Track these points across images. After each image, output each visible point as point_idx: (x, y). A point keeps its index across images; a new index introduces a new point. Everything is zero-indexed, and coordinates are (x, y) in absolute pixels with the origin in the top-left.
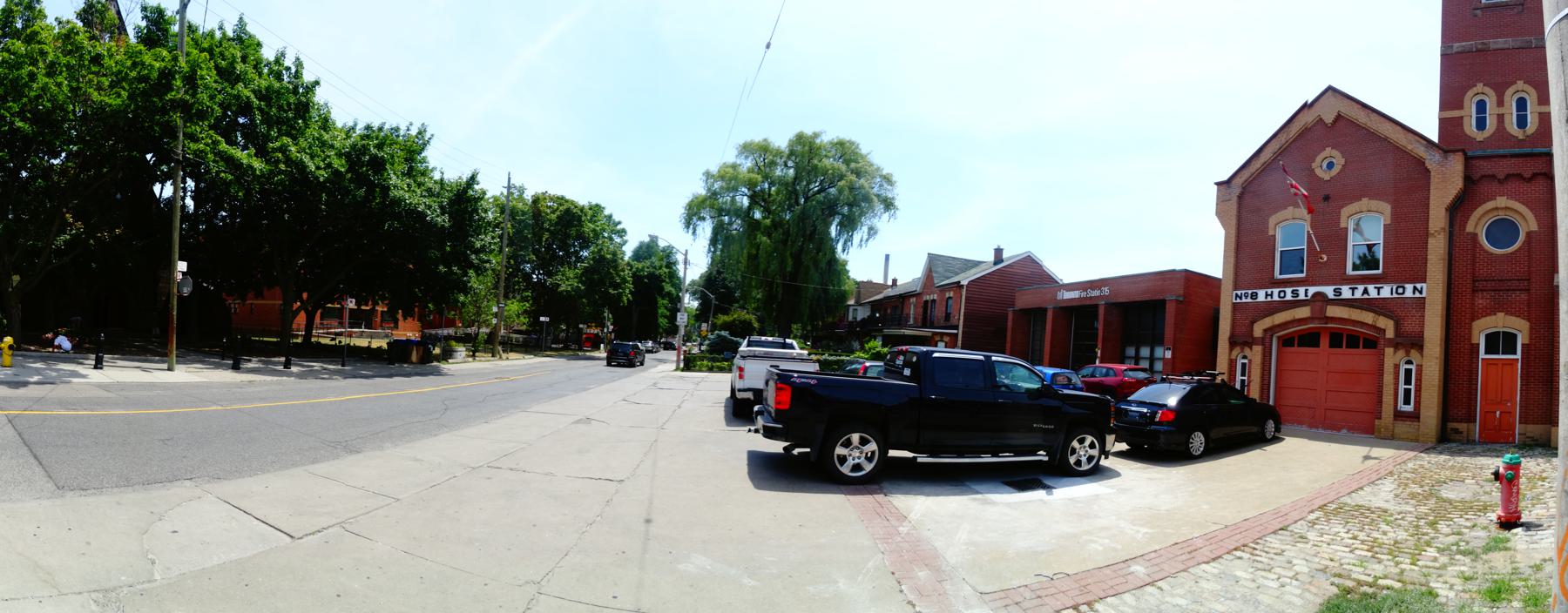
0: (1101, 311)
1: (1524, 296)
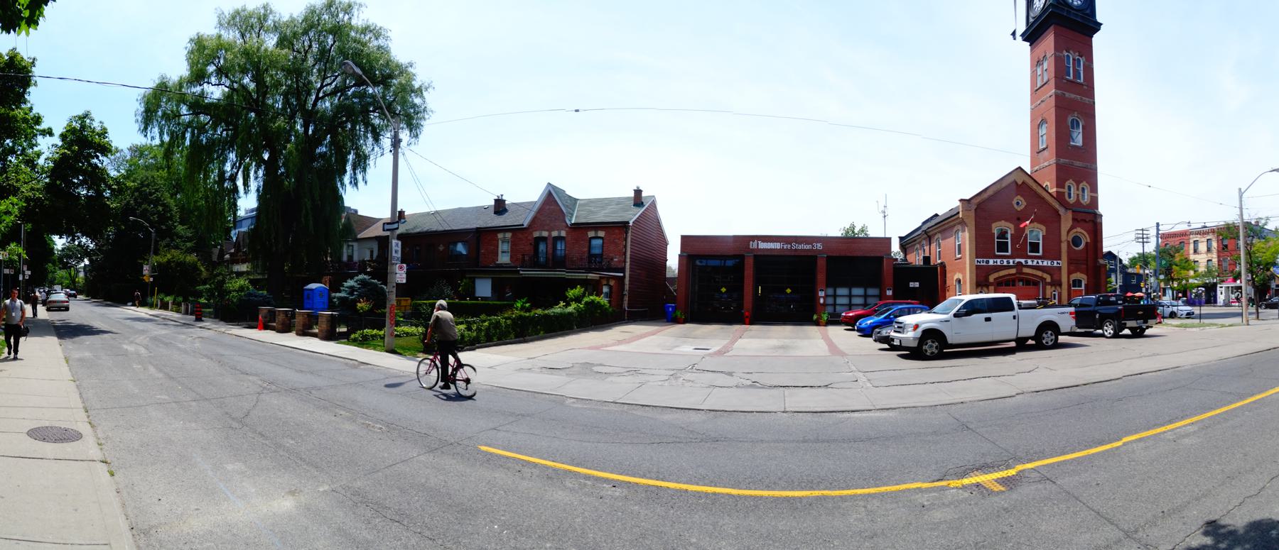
0: (821, 264)
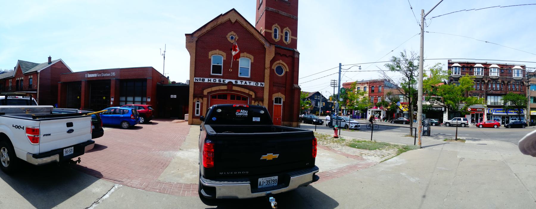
1: (284, 89)
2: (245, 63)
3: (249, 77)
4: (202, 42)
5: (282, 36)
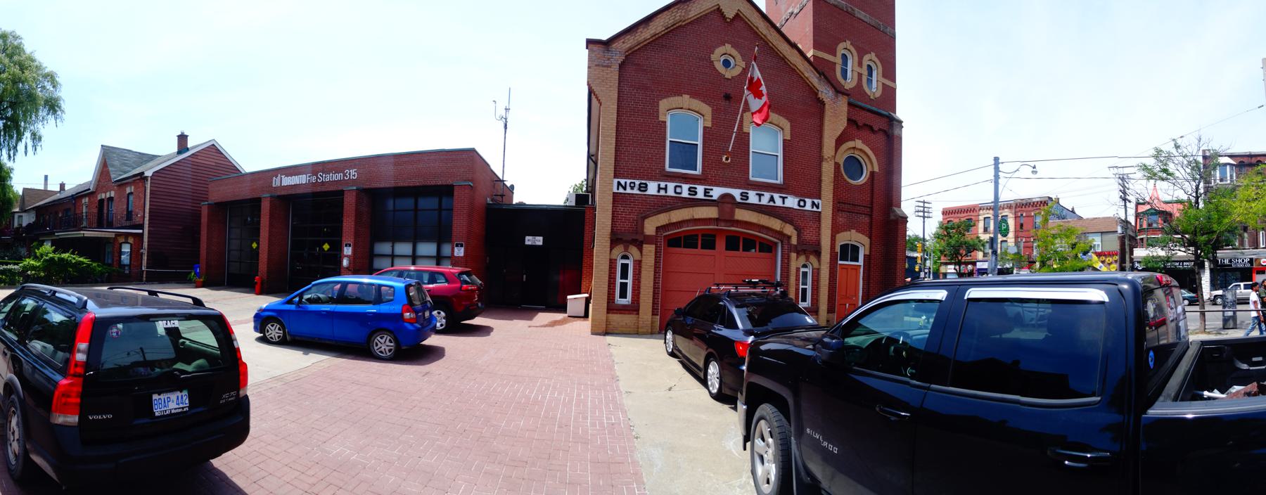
0: (349, 202)
2: (766, 143)
3: (780, 180)
4: (633, 72)
5: (860, 75)
